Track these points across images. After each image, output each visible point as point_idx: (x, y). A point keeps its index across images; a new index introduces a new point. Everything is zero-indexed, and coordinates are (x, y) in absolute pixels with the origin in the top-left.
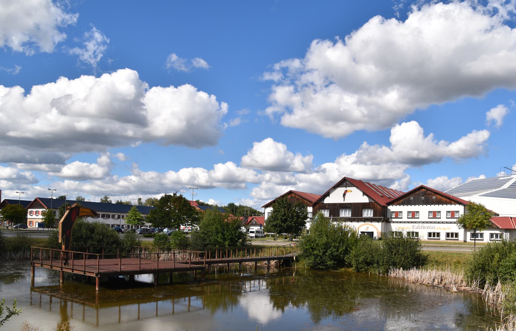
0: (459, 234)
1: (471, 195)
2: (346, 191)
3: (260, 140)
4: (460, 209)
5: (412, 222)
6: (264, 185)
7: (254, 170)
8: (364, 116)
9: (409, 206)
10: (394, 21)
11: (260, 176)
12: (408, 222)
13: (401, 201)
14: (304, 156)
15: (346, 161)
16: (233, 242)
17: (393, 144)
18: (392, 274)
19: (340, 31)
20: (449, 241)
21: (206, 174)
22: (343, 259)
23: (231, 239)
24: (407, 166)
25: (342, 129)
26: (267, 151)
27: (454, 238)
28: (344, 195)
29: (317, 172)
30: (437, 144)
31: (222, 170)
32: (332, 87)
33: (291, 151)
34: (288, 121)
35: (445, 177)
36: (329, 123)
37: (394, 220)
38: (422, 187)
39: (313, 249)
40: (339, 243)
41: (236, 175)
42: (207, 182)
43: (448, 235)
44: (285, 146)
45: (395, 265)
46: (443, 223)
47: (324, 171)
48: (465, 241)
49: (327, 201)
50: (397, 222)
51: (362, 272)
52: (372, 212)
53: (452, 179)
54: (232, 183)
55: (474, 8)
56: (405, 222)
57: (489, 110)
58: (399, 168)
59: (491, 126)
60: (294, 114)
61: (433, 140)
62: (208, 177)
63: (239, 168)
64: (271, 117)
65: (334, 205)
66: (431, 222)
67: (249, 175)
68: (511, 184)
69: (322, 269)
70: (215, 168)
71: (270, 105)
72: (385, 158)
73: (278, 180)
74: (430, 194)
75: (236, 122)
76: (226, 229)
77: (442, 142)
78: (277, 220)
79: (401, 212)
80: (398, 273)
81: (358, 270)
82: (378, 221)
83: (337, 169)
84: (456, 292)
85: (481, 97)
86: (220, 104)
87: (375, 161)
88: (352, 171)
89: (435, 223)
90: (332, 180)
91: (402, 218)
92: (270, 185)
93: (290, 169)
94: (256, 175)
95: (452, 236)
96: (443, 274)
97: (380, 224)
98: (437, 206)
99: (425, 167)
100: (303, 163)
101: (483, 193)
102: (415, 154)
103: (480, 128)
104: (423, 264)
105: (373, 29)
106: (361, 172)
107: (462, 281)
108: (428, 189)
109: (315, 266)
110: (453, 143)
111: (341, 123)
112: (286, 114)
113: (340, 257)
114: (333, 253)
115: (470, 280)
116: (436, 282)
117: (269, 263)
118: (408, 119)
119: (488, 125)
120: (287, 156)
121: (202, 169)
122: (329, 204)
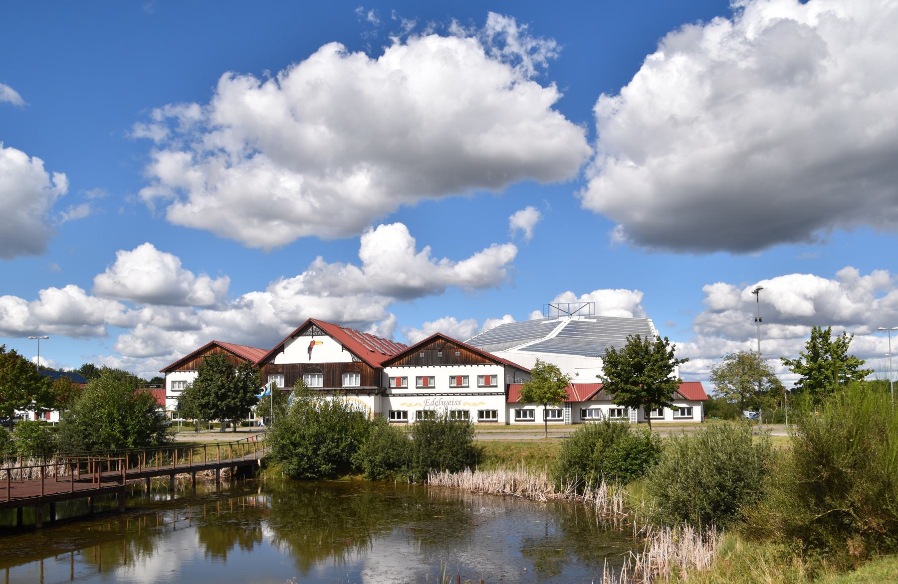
0: (499, 412)
1: (507, 348)
2: (313, 343)
3: (130, 247)
4: (499, 370)
5: (424, 395)
6: (140, 330)
7: (120, 302)
8: (315, 211)
9: (419, 368)
10: (362, 55)
11: (131, 313)
12: (418, 395)
13: (405, 359)
14: (214, 278)
15: (285, 288)
16: (142, 437)
17: (365, 262)
18: (434, 480)
19: (271, 62)
20: (483, 424)
21: (26, 309)
22: (348, 460)
23: (139, 433)
24: (390, 299)
25: (278, 233)
26: (143, 267)
27: (491, 419)
28: (310, 349)
29: (237, 307)
30: (436, 263)
31: (56, 300)
32: (258, 158)
33: (189, 269)
34: (179, 214)
35: (452, 319)
36: (255, 221)
37: (394, 391)
38: (437, 337)
39: (295, 445)
40: (340, 432)
41: (86, 312)
42: (26, 323)
43: (481, 414)
44: (178, 259)
45: (437, 466)
46: (472, 394)
47: (249, 305)
48: (508, 424)
49: (280, 359)
50: (400, 395)
51: (380, 480)
52: (359, 379)
53: (463, 322)
54: (76, 324)
55: (488, 53)
56: (412, 395)
57: (513, 213)
58: (376, 302)
59: (518, 237)
60: (190, 202)
61: (430, 258)
62: (28, 314)
63: (91, 298)
64: (152, 206)
65: (293, 366)
66: (454, 394)
67: (112, 311)
68: (560, 331)
69: (312, 479)
70: (42, 297)
71: (147, 183)
72: (351, 285)
73: (167, 321)
74: (451, 348)
75: (82, 211)
76: (123, 415)
77: (445, 261)
78: (209, 395)
79: (467, 377)
80: (441, 479)
81: (373, 476)
82: (368, 393)
83: (271, 303)
84: (545, 502)
85: (498, 192)
86: (51, 176)
87: (335, 290)
88: (298, 307)
89: (460, 394)
90: (262, 322)
91: (407, 388)
92: (152, 330)
93: (187, 301)
94: (125, 312)
95: (488, 416)
96: (517, 476)
97: (372, 398)
98: (462, 367)
99: (418, 301)
100: (212, 290)
101: (524, 346)
102: (400, 278)
103: (502, 239)
104: (479, 463)
105: (325, 65)
106: (315, 308)
107: (546, 485)
108: (447, 340)
109: (299, 474)
110: (460, 263)
111: (275, 223)
112: (176, 202)
113: (341, 457)
114: (330, 450)
115: (559, 484)
116: (507, 490)
117: (218, 472)
118: (390, 220)
119: (513, 236)
120: (182, 277)
121: (17, 298)
122: (283, 365)
